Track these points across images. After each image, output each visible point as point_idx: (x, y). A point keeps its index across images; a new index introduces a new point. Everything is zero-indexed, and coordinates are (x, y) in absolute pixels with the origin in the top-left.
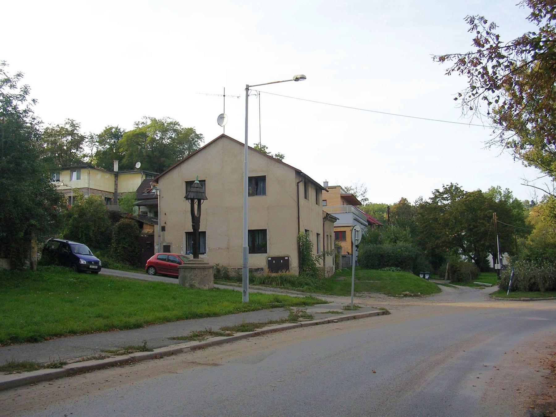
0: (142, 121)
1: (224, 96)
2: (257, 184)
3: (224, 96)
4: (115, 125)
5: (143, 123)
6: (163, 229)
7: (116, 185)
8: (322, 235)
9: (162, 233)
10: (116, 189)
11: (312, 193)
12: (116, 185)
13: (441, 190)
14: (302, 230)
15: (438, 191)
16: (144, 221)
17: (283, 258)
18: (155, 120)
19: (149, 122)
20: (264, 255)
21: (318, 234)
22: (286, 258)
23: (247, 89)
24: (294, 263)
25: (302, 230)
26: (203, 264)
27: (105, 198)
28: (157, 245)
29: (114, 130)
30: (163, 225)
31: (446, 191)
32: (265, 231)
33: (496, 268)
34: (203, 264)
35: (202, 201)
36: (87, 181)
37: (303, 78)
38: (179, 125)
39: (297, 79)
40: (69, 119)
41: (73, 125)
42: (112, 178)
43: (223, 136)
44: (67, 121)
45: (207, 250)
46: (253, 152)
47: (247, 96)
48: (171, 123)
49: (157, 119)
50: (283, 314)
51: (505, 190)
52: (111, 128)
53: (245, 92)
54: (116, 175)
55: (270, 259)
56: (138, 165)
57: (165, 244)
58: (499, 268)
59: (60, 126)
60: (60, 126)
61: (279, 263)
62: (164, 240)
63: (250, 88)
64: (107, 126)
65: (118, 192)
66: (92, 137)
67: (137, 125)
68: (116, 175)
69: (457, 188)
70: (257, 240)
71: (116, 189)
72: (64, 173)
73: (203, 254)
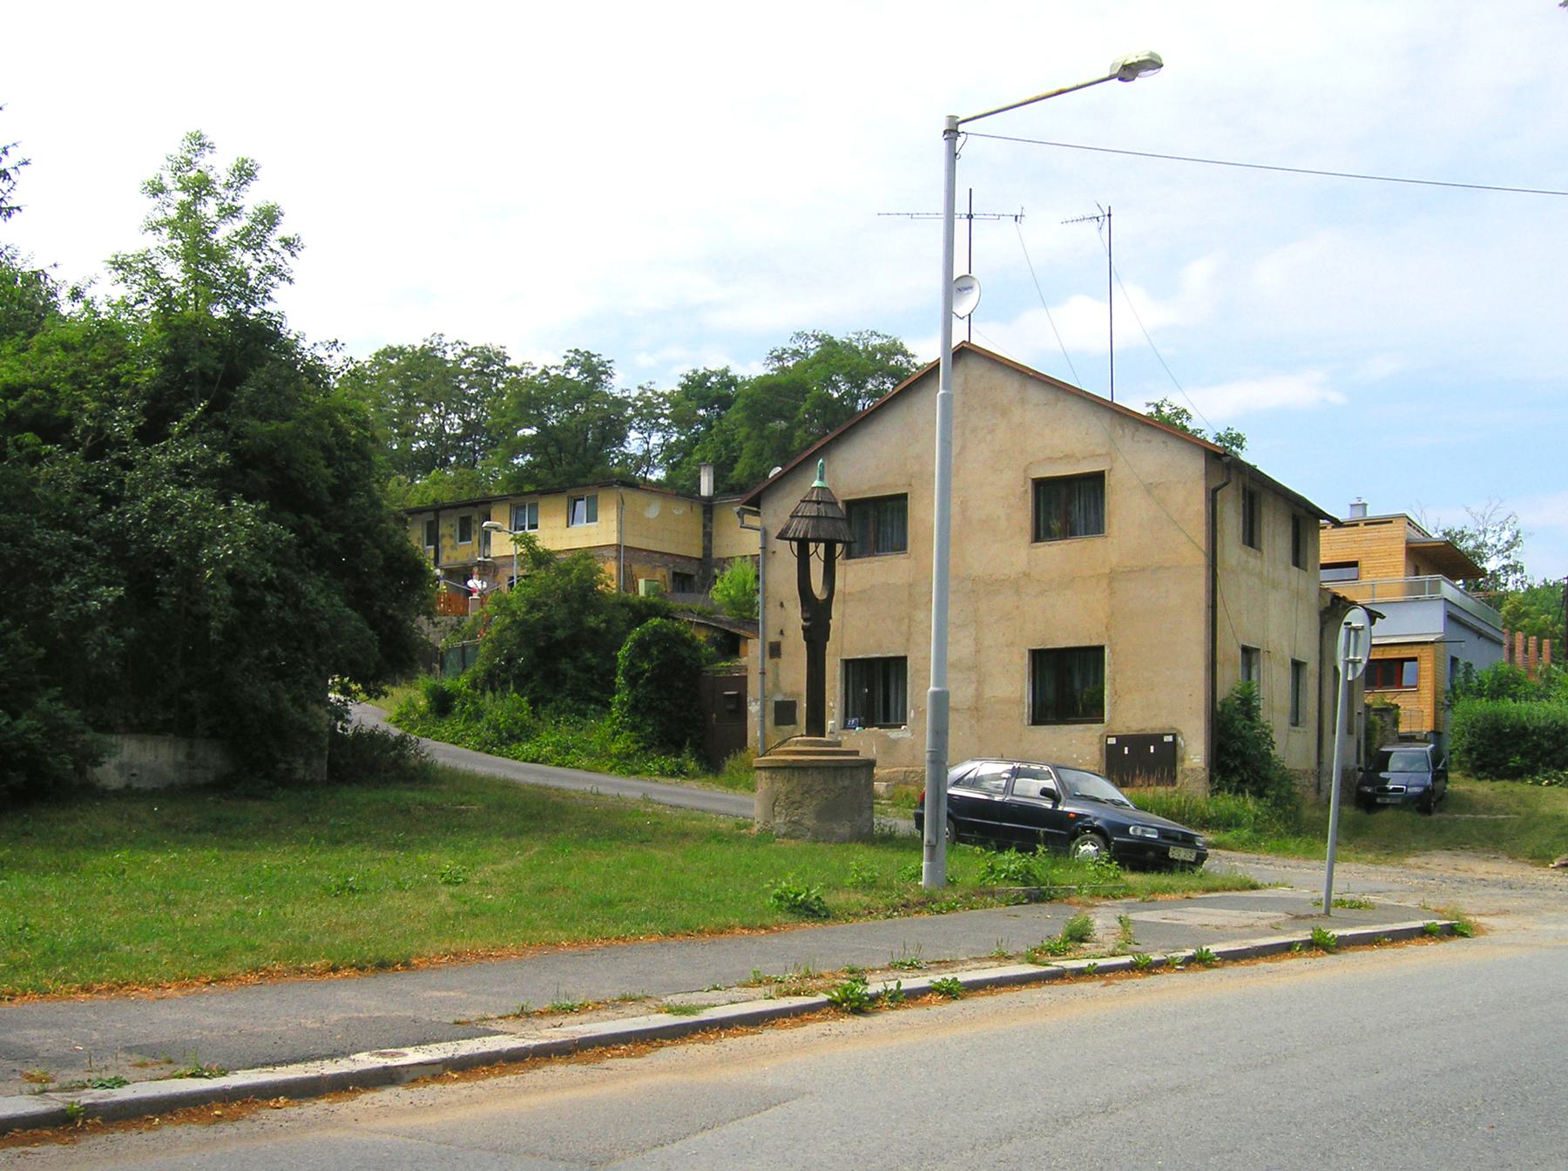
1: (970, 217)
2: (1067, 505)
3: (970, 217)
5: (796, 353)
7: (708, 536)
8: (1312, 666)
9: (769, 663)
10: (707, 549)
11: (1276, 535)
12: (708, 536)
14: (1229, 650)
16: (742, 632)
17: (1156, 738)
20: (1096, 729)
21: (1297, 666)
22: (1168, 739)
23: (952, 133)
24: (1195, 755)
25: (1229, 650)
27: (675, 574)
28: (756, 700)
30: (773, 637)
36: (614, 525)
37: (1153, 64)
38: (905, 354)
39: (1128, 72)
40: (577, 351)
42: (698, 510)
45: (911, 714)
46: (1143, 433)
47: (953, 156)
48: (881, 349)
49: (837, 339)
50: (1179, 896)
52: (706, 377)
53: (943, 145)
55: (1112, 741)
57: (779, 698)
59: (553, 372)
60: (553, 372)
61: (1143, 758)
62: (777, 685)
63: (961, 128)
65: (715, 555)
67: (779, 358)
68: (708, 508)
70: (1066, 683)
71: (707, 549)
72: (545, 505)
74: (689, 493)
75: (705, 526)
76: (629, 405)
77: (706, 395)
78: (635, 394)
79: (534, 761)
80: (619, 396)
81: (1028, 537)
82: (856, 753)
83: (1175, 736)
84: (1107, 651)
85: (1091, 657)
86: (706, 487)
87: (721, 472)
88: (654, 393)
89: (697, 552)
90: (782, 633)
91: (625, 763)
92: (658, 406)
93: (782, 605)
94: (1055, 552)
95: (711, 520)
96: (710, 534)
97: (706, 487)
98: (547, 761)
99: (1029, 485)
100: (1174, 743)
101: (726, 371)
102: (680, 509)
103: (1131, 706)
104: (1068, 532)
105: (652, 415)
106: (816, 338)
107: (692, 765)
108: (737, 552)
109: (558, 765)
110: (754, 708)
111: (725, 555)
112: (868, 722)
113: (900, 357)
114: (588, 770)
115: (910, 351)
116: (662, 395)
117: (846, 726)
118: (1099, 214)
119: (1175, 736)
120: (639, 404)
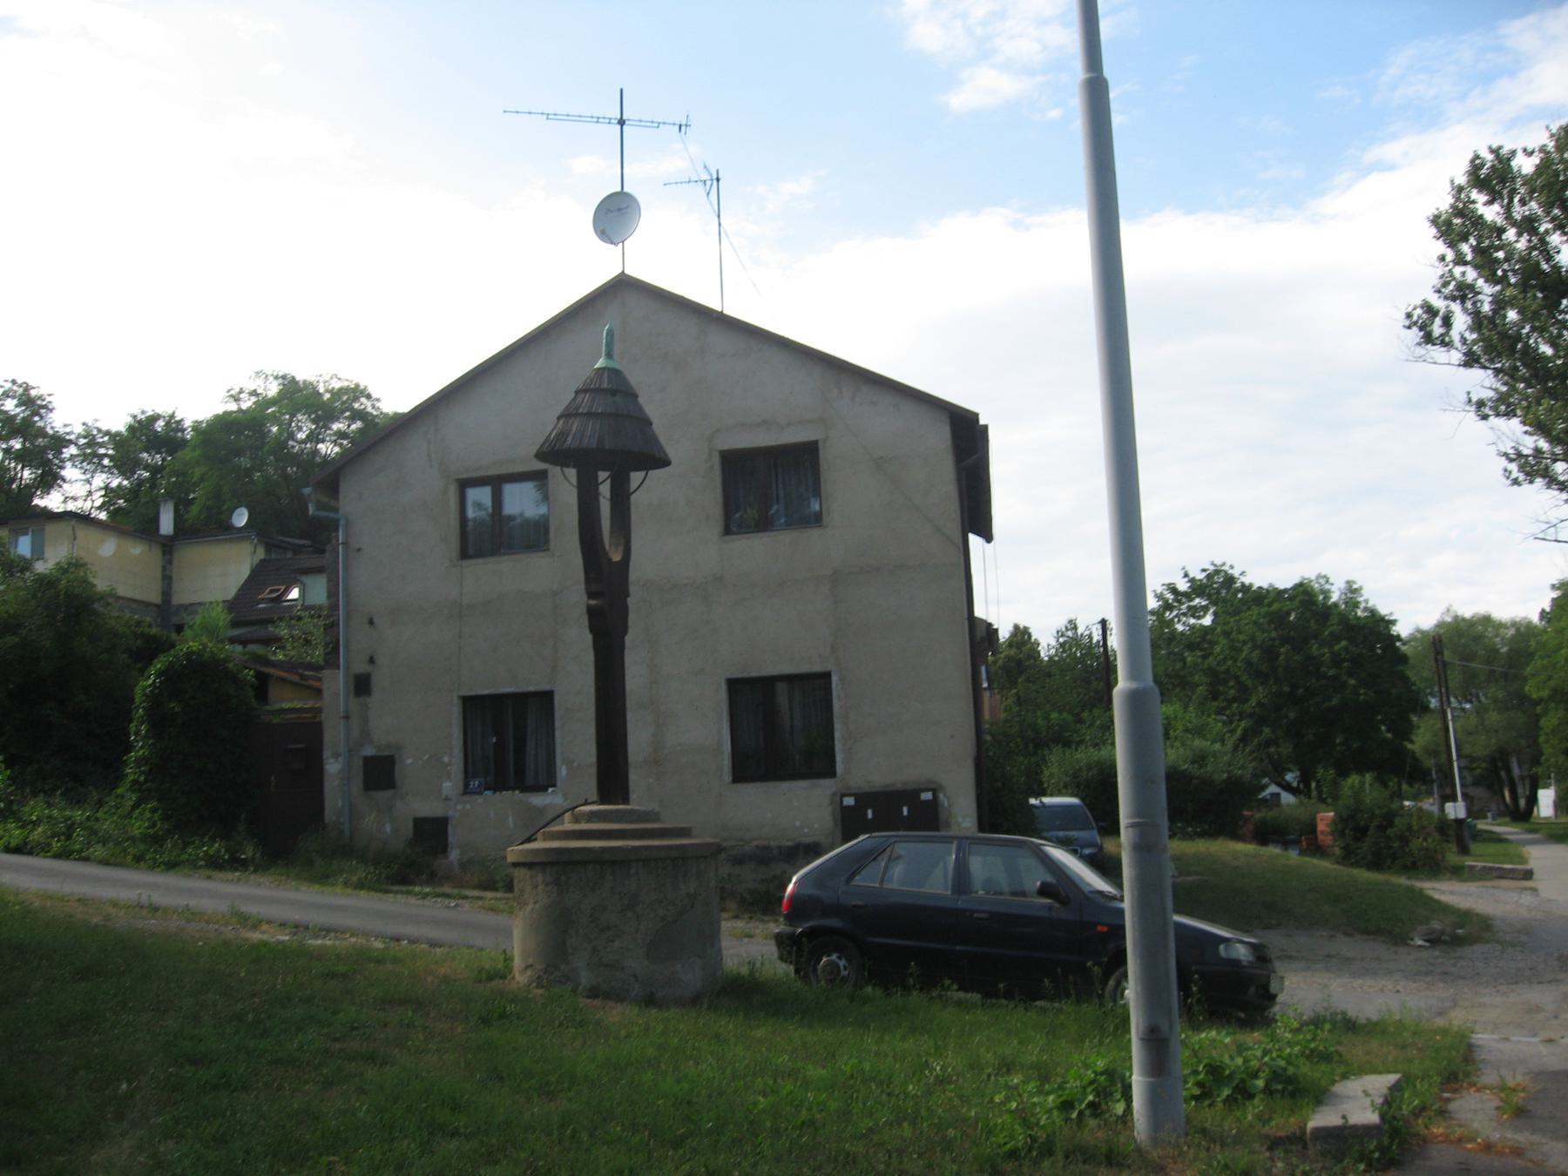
0: (250, 386)
1: (622, 122)
3: (622, 122)
4: (164, 408)
5: (254, 393)
6: (362, 685)
7: (167, 579)
10: (167, 594)
12: (167, 579)
13: (1183, 586)
15: (1173, 589)
18: (293, 381)
19: (273, 389)
20: (825, 787)
22: (926, 796)
26: (664, 833)
28: (336, 755)
29: (159, 425)
30: (360, 667)
31: (1198, 588)
32: (826, 676)
33: (1452, 816)
34: (664, 833)
35: (636, 477)
38: (369, 397)
40: (14, 382)
41: (28, 401)
42: (155, 555)
43: (623, 286)
44: (8, 385)
45: (562, 772)
48: (342, 391)
51: (1343, 586)
52: (154, 418)
54: (168, 547)
55: (849, 801)
56: (241, 518)
57: (369, 751)
58: (1462, 814)
62: (366, 735)
64: (137, 412)
65: (177, 599)
66: (92, 443)
67: (236, 399)
68: (168, 547)
69: (1230, 580)
71: (167, 594)
73: (543, 789)
74: (146, 529)
75: (164, 568)
76: (70, 442)
77: (146, 442)
78: (79, 429)
79: (17, 850)
80: (62, 431)
81: (717, 527)
82: (684, 832)
83: (935, 791)
84: (834, 678)
85: (815, 686)
86: (167, 524)
87: (182, 506)
88: (99, 431)
89: (154, 597)
90: (371, 660)
91: (148, 852)
92: (102, 445)
93: (371, 622)
94: (754, 549)
95: (170, 562)
96: (170, 578)
97: (167, 524)
98: (41, 849)
99: (716, 460)
100: (935, 802)
101: (172, 416)
102: (137, 549)
103: (868, 758)
104: (764, 524)
105: (95, 455)
106: (276, 378)
107: (248, 852)
108: (208, 598)
109: (57, 856)
110: (332, 767)
111: (195, 599)
112: (499, 785)
113: (363, 400)
114: (105, 863)
115: (374, 396)
116: (107, 433)
117: (467, 791)
118: (705, 177)
119: (935, 791)
120: (82, 441)
